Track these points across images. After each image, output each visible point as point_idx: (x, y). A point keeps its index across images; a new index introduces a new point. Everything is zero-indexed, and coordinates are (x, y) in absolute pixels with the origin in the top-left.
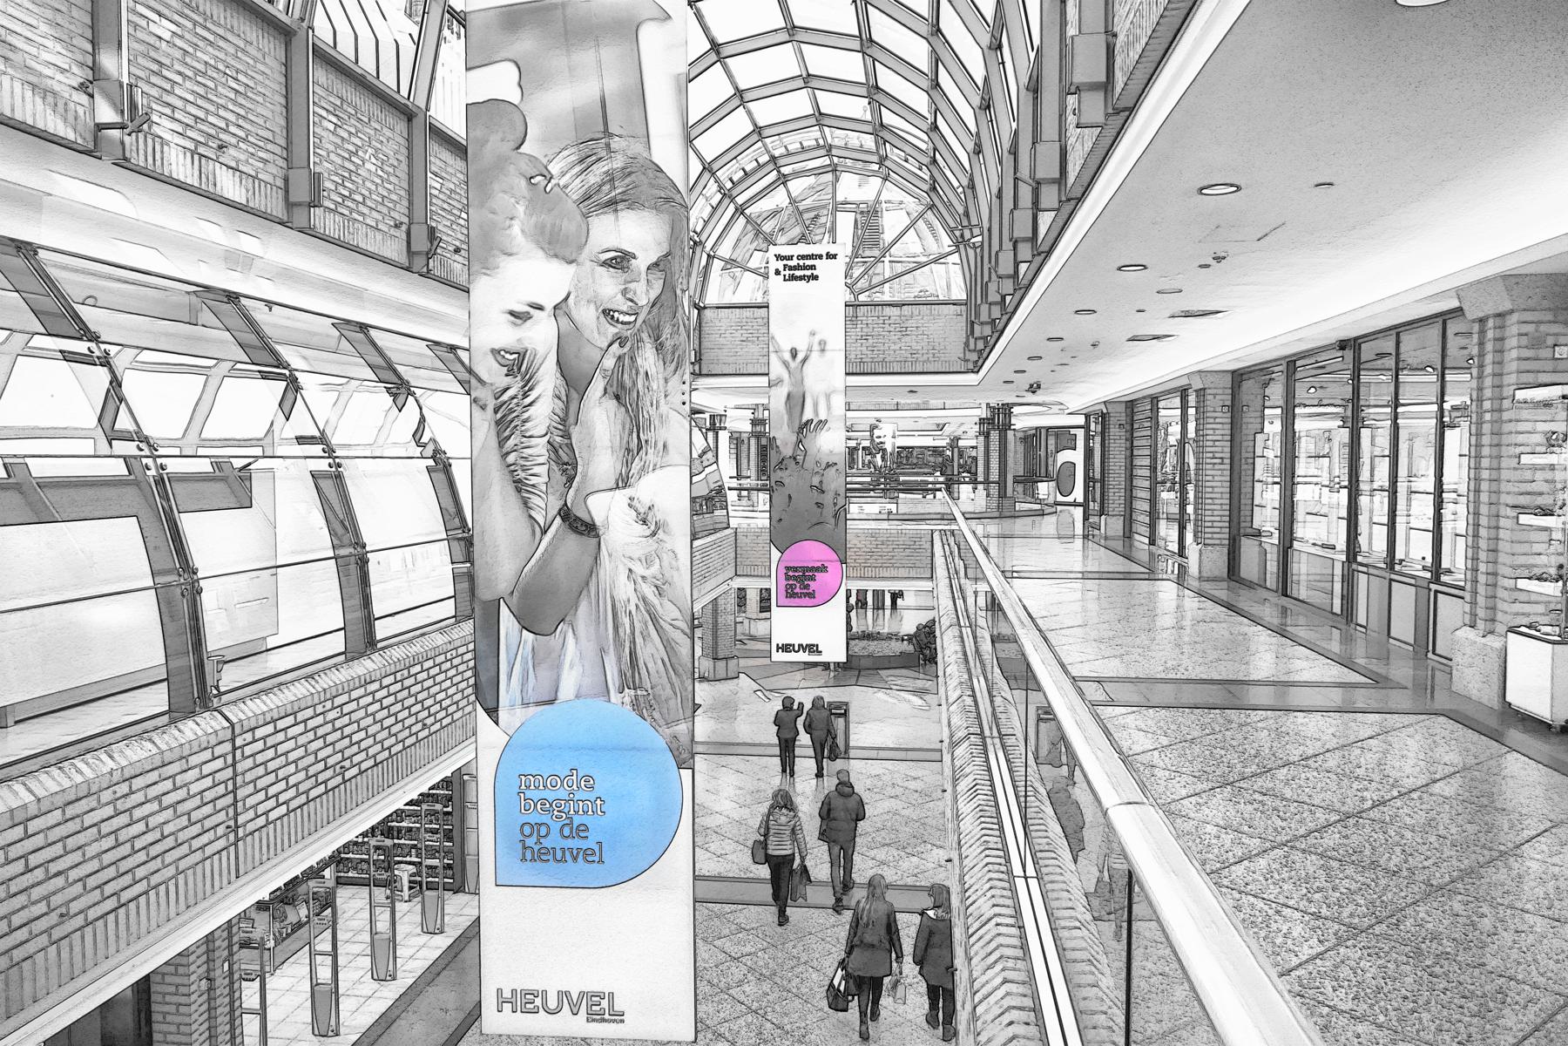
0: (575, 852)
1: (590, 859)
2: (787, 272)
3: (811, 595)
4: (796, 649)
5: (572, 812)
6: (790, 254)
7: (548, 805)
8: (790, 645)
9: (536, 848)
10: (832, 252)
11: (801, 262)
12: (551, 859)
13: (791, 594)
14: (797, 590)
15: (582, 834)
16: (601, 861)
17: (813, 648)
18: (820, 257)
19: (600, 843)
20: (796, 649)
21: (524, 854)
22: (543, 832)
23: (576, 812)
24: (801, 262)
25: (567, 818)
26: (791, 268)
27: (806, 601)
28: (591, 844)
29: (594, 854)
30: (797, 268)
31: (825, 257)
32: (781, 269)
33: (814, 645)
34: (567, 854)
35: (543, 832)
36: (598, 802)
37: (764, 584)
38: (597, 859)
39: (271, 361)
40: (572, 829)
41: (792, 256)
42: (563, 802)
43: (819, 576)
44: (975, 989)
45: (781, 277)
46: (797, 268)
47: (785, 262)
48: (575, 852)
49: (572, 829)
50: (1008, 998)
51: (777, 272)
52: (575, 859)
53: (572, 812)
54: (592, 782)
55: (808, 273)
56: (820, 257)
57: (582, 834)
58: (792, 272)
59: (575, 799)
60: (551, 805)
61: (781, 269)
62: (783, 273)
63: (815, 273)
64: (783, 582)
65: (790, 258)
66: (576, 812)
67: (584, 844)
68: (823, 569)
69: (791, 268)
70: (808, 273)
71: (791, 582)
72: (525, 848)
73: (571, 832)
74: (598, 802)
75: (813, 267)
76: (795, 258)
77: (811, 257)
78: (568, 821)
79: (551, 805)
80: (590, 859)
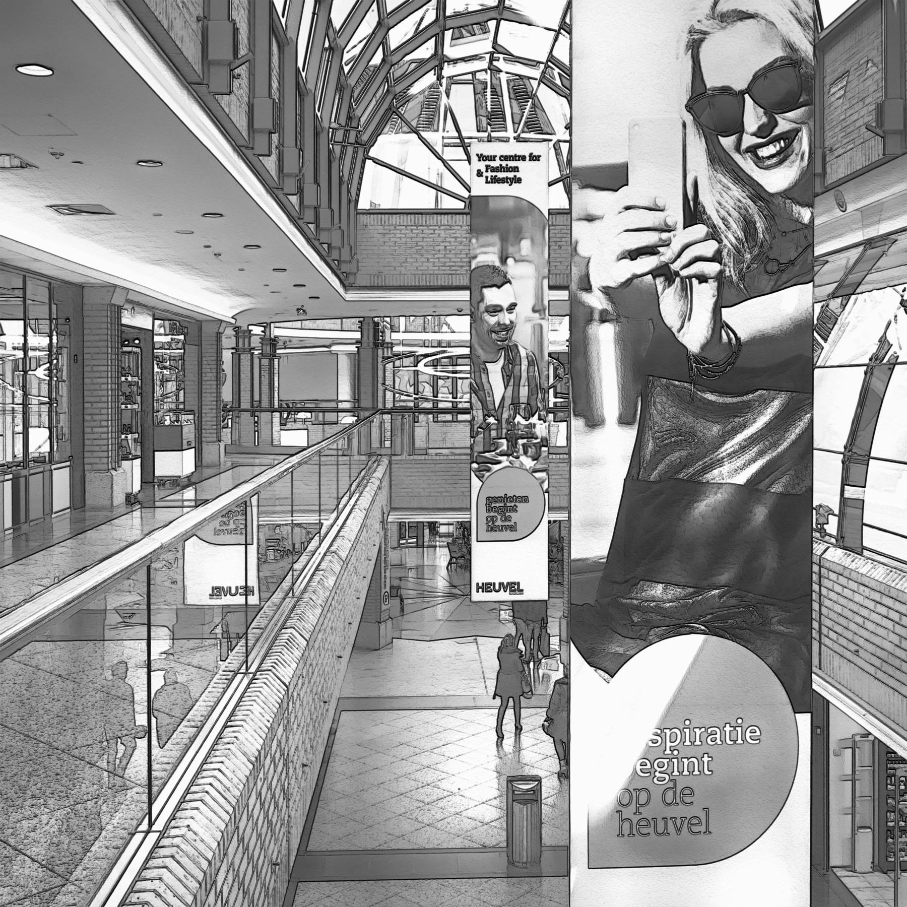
0: (679, 822)
1: (695, 829)
2: (489, 174)
3: (513, 528)
4: (497, 588)
5: (676, 773)
6: (493, 154)
7: (649, 766)
8: (490, 584)
9: (635, 819)
10: (535, 153)
11: (504, 164)
12: (650, 819)
13: (491, 528)
14: (499, 523)
15: (688, 799)
16: (708, 832)
17: (514, 587)
18: (523, 158)
19: (706, 809)
20: (497, 588)
21: (621, 828)
22: (643, 800)
23: (681, 773)
24: (504, 164)
25: (670, 780)
26: (493, 170)
27: (507, 534)
28: (696, 810)
29: (700, 823)
30: (500, 169)
31: (528, 158)
32: (483, 169)
33: (515, 583)
34: (670, 823)
35: (643, 800)
36: (706, 759)
37: (462, 517)
38: (703, 828)
39: (563, 78)
40: (675, 793)
41: (495, 156)
42: (665, 761)
43: (521, 506)
44: (147, 866)
45: (483, 179)
46: (500, 169)
47: (487, 163)
48: (679, 822)
49: (675, 793)
50: (165, 870)
51: (479, 174)
52: (678, 830)
53: (676, 773)
54: (758, 733)
55: (511, 175)
56: (523, 158)
57: (688, 799)
58: (494, 174)
59: (680, 757)
60: (652, 766)
61: (483, 169)
62: (485, 174)
63: (518, 175)
64: (484, 514)
65: (493, 158)
66: (681, 773)
67: (688, 812)
68: (525, 499)
69: (493, 170)
70: (511, 175)
71: (492, 514)
72: (622, 820)
73: (675, 798)
74: (706, 759)
75: (516, 169)
76: (497, 158)
77: (515, 158)
78: (671, 785)
79: (652, 766)
80: (695, 829)
